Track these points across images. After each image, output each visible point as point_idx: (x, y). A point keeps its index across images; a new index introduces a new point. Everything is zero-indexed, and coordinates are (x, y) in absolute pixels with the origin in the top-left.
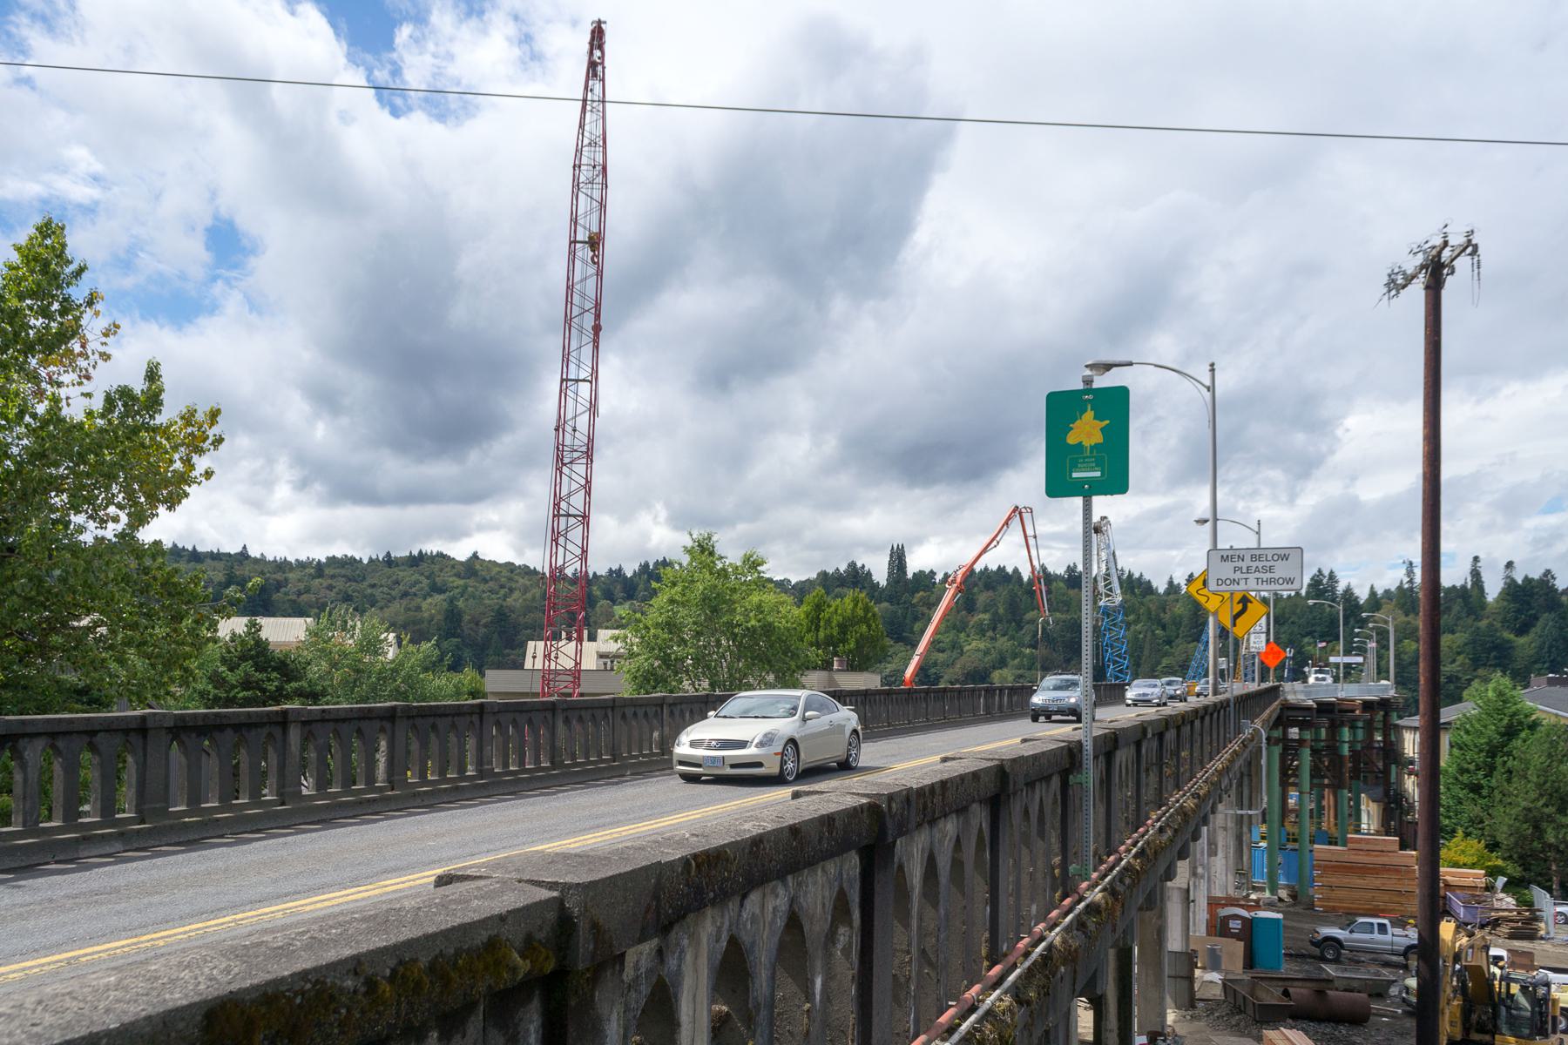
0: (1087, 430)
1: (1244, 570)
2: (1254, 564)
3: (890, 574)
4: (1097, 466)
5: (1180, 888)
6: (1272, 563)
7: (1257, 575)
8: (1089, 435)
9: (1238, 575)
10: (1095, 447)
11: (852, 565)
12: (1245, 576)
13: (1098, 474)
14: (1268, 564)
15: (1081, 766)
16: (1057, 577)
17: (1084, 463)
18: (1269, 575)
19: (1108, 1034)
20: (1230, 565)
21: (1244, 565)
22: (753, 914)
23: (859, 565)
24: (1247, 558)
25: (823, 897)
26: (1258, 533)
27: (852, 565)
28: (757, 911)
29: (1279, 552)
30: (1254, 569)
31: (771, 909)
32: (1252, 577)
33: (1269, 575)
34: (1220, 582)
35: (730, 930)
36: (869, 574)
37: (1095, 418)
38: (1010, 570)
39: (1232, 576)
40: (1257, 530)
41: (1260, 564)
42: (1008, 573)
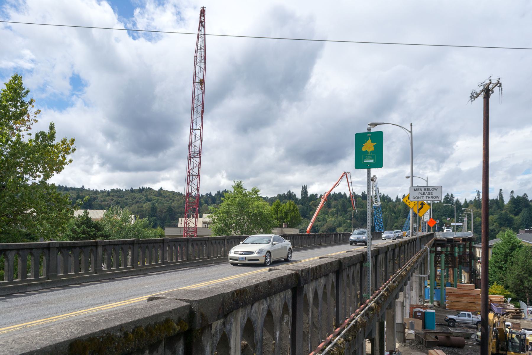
0: (369, 146)
1: (422, 194)
2: (426, 192)
3: (302, 195)
4: (372, 158)
5: (400, 302)
6: (431, 191)
7: (427, 195)
8: (370, 148)
9: (420, 195)
10: (372, 152)
11: (289, 192)
12: (422, 196)
13: (373, 161)
14: (430, 192)
15: (367, 260)
16: (359, 196)
17: (368, 157)
18: (430, 195)
19: (376, 351)
20: (417, 192)
21: (422, 192)
22: (256, 311)
23: (291, 192)
24: (423, 190)
25: (279, 305)
26: (427, 181)
27: (289, 192)
28: (257, 310)
29: (434, 187)
30: (425, 193)
31: (261, 309)
32: (425, 196)
33: (430, 195)
34: (414, 198)
35: (248, 316)
36: (295, 195)
37: (372, 142)
38: (343, 194)
39: (418, 196)
40: (426, 180)
41: (428, 192)
42: (342, 195)
